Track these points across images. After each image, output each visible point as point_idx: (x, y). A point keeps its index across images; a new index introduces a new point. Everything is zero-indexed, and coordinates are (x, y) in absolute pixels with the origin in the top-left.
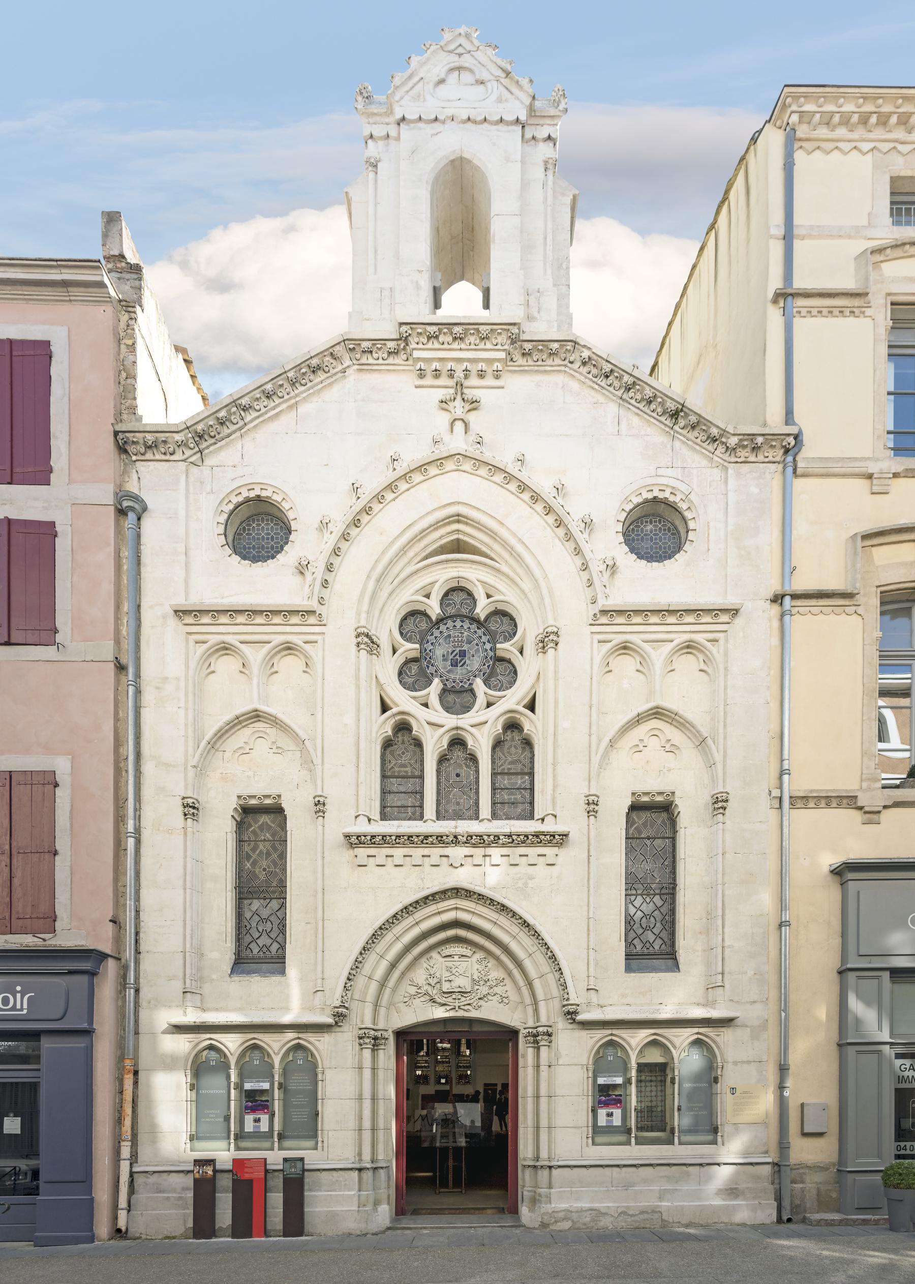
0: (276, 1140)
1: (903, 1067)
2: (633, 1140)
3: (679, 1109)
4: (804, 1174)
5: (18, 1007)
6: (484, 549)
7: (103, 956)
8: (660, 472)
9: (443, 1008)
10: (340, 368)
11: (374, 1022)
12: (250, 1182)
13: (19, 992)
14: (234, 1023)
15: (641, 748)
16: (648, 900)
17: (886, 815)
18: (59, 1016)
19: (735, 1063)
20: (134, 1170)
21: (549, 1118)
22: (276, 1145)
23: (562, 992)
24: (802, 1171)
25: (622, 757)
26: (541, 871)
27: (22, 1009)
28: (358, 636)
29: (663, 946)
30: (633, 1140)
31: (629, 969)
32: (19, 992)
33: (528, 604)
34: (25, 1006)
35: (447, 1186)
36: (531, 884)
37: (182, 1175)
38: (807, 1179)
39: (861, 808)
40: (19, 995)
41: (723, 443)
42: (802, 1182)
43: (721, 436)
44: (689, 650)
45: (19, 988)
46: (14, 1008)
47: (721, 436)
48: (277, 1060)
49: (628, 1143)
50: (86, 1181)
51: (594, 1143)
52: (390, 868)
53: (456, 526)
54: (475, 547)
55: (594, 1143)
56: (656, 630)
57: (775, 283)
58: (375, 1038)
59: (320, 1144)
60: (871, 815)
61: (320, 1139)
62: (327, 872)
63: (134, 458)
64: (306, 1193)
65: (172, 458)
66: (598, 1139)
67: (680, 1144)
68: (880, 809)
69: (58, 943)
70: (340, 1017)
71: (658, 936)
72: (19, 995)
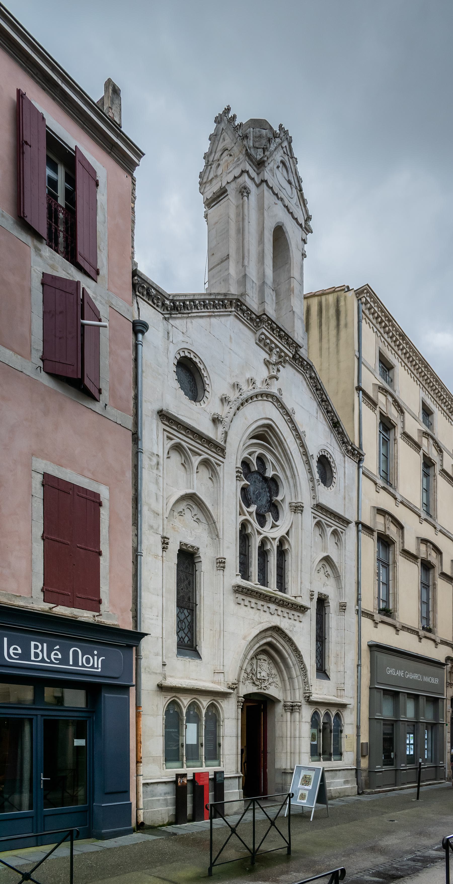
0: (204, 760)
2: (322, 759)
5: (96, 666)
6: (273, 445)
9: (256, 688)
12: (202, 787)
13: (96, 655)
14: (208, 689)
15: (183, 514)
16: (182, 611)
21: (299, 748)
22: (204, 764)
23: (304, 686)
26: (297, 623)
27: (97, 668)
29: (189, 642)
30: (322, 759)
31: (179, 653)
32: (96, 655)
33: (287, 483)
34: (100, 666)
36: (295, 629)
37: (164, 785)
40: (96, 657)
41: (346, 446)
43: (347, 443)
44: (205, 464)
45: (96, 652)
46: (93, 667)
47: (347, 443)
48: (184, 711)
49: (319, 760)
52: (242, 606)
53: (266, 429)
54: (269, 440)
56: (196, 446)
57: (356, 385)
58: (292, 706)
59: (222, 763)
61: (221, 760)
62: (225, 603)
63: (138, 293)
64: (225, 792)
65: (157, 308)
69: (103, 620)
71: (186, 635)
72: (96, 657)
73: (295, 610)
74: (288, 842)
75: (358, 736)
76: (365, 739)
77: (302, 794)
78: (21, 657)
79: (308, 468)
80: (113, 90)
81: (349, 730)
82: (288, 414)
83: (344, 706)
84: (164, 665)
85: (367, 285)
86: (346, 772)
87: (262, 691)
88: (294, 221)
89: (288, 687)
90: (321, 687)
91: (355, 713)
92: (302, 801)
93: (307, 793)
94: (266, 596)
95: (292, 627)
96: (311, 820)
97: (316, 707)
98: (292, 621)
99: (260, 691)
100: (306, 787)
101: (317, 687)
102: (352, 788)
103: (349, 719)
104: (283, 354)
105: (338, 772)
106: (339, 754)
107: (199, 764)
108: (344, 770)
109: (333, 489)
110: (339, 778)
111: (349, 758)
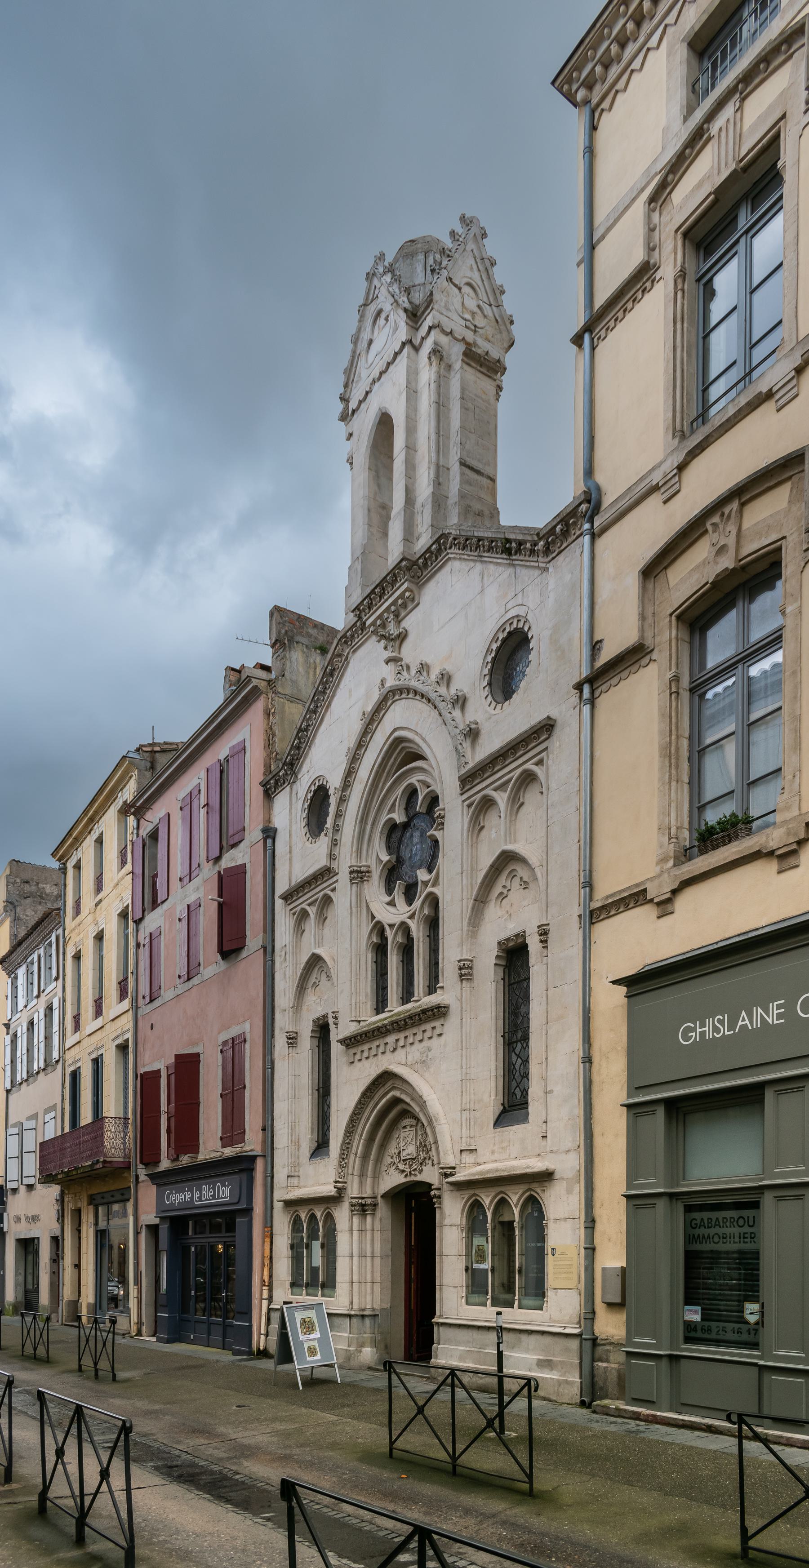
1: (694, 1222)
2: (489, 1302)
3: (520, 1271)
4: (608, 1351)
7: (254, 1158)
8: (510, 606)
10: (344, 658)
11: (361, 1191)
17: (683, 902)
18: (236, 1201)
19: (555, 1220)
20: (271, 1307)
24: (608, 1347)
25: (493, 911)
28: (351, 873)
35: (758, 1264)
36: (430, 1055)
38: (612, 1357)
39: (651, 901)
42: (607, 1361)
50: (247, 1313)
51: (467, 1303)
52: (357, 1063)
55: (467, 1303)
60: (665, 906)
66: (471, 1300)
67: (520, 1307)
68: (794, 846)
70: (341, 1191)
73: (428, 1020)
74: (528, 1471)
75: (591, 1250)
76: (613, 1257)
77: (310, 1348)
78: (214, 1197)
79: (343, 808)
80: (578, 265)
81: (562, 1235)
82: (371, 721)
83: (546, 1177)
84: (544, 1137)
85: (553, 83)
86: (548, 1339)
87: (412, 1178)
88: (391, 368)
89: (370, 1172)
90: (504, 1145)
91: (579, 1189)
92: (315, 1358)
93: (315, 1344)
94: (373, 1031)
95: (425, 1055)
96: (301, 1388)
97: (472, 1192)
98: (417, 1045)
99: (408, 1179)
100: (312, 1336)
101: (496, 1148)
102: (559, 1383)
103: (561, 1206)
104: (400, 602)
105: (524, 1337)
106: (537, 1291)
107: (482, 1299)
108: (543, 1333)
109: (490, 710)
110: (527, 1350)
111: (561, 1307)
